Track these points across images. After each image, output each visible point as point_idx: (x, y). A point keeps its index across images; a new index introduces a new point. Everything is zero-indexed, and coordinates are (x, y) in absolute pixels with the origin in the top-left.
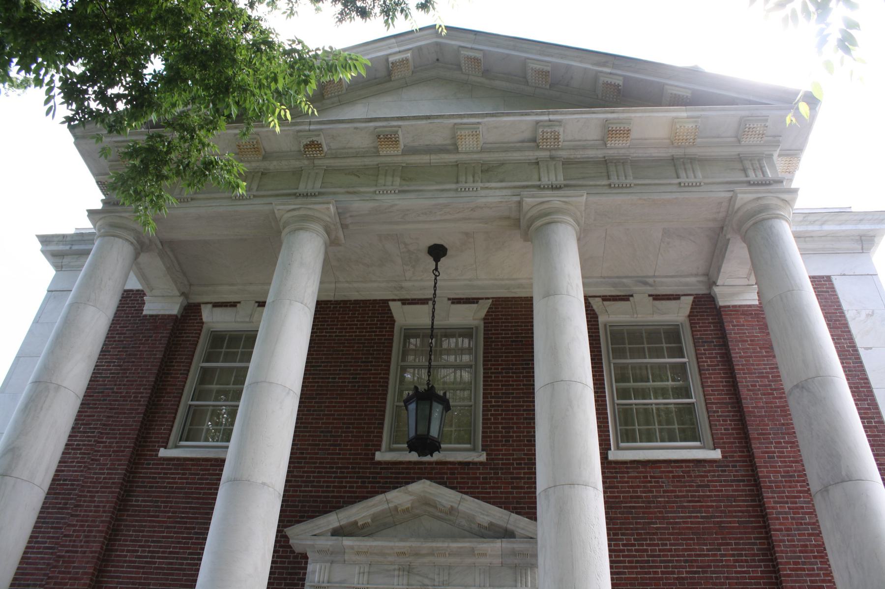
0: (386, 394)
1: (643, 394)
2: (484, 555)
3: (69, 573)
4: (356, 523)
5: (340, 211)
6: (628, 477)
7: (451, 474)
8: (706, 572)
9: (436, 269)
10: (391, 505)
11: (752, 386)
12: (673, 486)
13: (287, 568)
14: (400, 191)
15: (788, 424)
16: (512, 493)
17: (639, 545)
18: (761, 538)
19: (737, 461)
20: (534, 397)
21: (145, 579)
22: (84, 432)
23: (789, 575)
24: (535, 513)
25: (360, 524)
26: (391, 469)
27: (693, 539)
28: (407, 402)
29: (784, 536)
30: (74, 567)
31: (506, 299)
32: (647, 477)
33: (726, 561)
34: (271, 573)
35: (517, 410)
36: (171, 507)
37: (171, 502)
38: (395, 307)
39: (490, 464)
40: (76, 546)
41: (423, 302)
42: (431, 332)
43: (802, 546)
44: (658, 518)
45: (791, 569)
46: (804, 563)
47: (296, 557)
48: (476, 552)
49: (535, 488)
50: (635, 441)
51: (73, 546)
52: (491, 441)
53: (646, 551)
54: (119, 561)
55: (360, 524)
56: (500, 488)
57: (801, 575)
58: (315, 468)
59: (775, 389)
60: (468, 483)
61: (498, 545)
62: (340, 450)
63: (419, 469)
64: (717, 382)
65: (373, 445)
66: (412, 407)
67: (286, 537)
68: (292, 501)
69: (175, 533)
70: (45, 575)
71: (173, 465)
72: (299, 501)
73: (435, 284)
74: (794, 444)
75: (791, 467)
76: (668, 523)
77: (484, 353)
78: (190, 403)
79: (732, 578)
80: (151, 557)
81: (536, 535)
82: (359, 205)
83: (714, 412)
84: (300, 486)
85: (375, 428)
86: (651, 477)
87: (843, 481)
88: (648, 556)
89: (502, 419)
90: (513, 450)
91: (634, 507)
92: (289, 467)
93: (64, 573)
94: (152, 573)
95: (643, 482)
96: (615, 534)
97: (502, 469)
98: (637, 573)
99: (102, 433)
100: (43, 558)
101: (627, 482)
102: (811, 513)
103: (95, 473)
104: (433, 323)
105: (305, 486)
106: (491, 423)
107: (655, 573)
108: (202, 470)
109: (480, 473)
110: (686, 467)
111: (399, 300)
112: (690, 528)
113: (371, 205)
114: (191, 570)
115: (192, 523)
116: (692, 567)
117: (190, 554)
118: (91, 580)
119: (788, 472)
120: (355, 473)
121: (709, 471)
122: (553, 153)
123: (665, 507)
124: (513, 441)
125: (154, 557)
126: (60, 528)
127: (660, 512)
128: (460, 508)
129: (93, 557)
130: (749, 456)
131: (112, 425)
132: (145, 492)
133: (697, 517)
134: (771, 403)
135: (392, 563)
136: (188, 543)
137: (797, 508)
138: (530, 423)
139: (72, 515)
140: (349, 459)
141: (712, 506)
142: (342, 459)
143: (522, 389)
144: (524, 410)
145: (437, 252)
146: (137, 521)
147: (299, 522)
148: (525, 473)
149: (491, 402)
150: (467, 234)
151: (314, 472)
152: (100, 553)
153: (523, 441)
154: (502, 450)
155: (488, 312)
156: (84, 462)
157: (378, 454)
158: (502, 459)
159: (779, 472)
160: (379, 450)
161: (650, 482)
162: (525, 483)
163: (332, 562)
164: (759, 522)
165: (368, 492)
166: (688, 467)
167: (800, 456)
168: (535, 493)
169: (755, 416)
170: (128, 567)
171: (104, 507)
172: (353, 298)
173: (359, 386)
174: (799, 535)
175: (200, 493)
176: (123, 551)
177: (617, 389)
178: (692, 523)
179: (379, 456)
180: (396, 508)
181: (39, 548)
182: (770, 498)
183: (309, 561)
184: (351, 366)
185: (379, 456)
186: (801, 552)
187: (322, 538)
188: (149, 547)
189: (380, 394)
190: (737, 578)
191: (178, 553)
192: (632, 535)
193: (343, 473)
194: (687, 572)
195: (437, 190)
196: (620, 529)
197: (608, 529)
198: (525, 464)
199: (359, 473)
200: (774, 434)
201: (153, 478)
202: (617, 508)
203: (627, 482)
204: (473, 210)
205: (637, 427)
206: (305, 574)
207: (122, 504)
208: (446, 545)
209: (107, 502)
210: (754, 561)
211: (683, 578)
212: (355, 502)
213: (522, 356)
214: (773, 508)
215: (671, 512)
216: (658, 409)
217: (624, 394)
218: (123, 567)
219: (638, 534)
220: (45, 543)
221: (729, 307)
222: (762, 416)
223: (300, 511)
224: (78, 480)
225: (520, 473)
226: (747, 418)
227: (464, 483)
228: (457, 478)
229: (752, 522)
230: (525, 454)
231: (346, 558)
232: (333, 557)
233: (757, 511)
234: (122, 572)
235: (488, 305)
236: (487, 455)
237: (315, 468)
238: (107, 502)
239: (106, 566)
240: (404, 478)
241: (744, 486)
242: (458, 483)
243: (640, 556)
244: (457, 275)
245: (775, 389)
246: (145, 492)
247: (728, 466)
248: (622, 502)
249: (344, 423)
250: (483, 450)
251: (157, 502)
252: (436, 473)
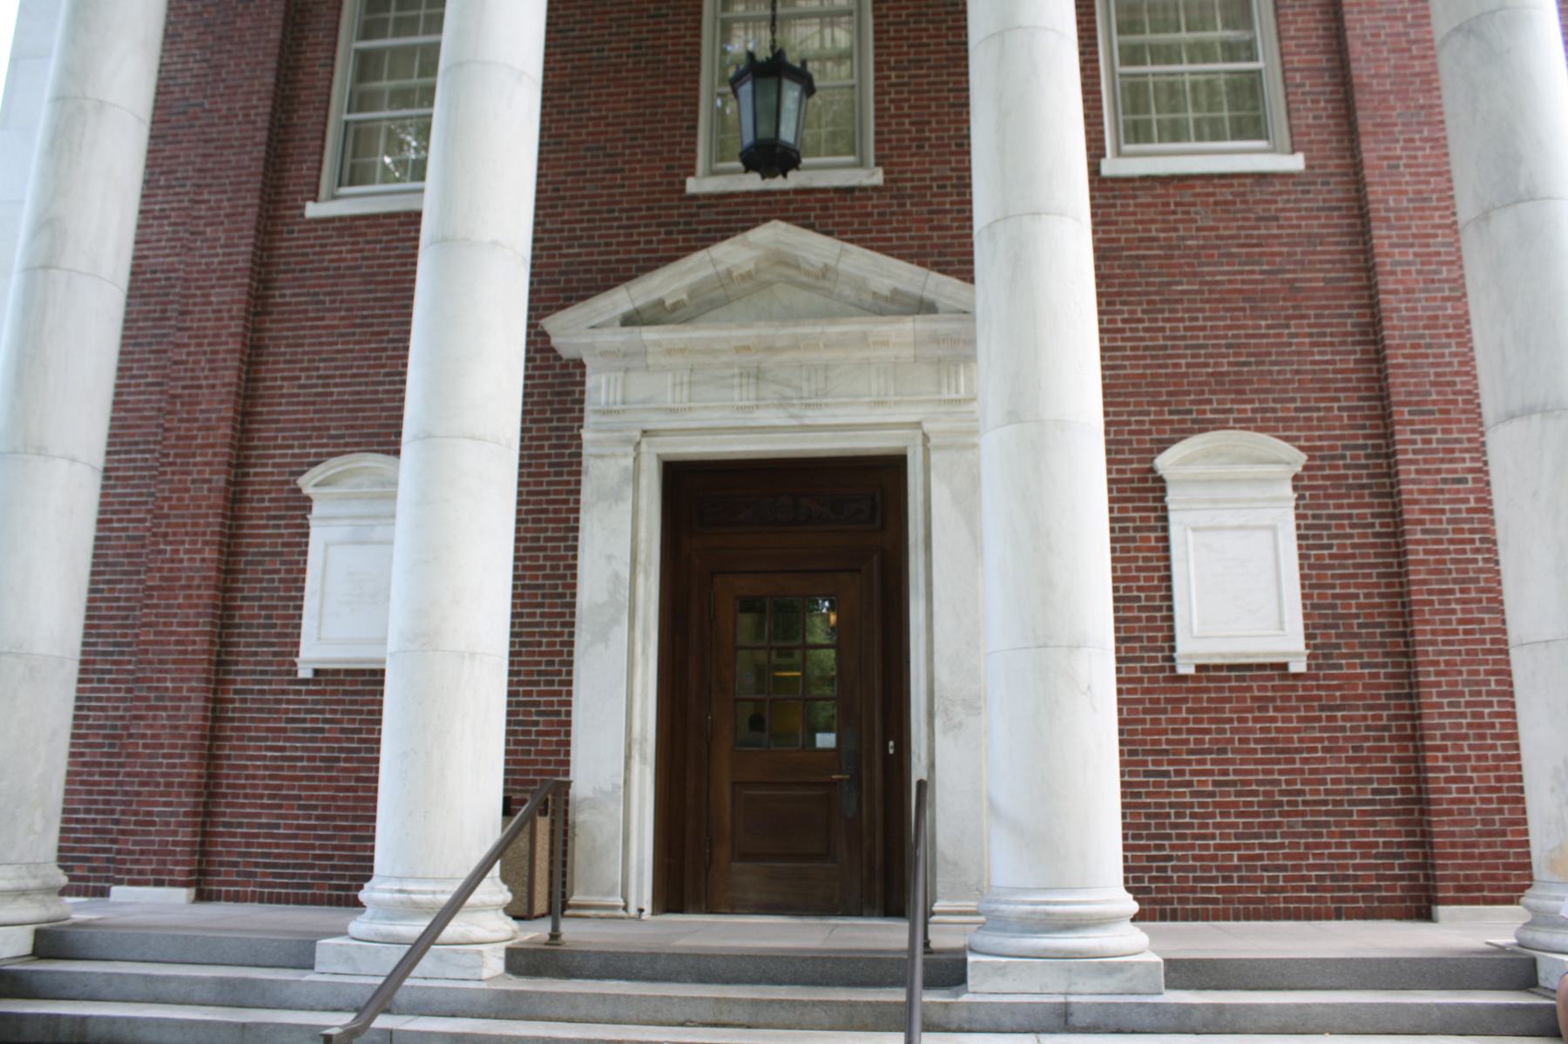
0: (697, 74)
1: (1168, 54)
2: (885, 344)
3: (196, 420)
4: (661, 302)
6: (1136, 205)
8: (1262, 363)
10: (721, 268)
11: (1373, 35)
12: (1215, 220)
13: (552, 385)
15: (1431, 106)
16: (930, 238)
17: (1151, 320)
18: (1360, 306)
19: (1332, 175)
20: (967, 66)
21: (320, 420)
22: (169, 187)
23: (1401, 366)
24: (971, 272)
25: (668, 303)
27: (1243, 309)
28: (735, 83)
29: (1401, 301)
30: (202, 411)
32: (1168, 204)
33: (1298, 344)
34: (526, 395)
36: (342, 301)
37: (340, 293)
39: (891, 189)
40: (198, 378)
43: (1430, 318)
45: (1406, 356)
46: (1429, 346)
47: (565, 366)
48: (871, 340)
49: (971, 228)
50: (1149, 140)
51: (192, 378)
52: (891, 149)
53: (1163, 329)
54: (272, 396)
55: (668, 303)
56: (908, 230)
57: (1421, 366)
58: (582, 213)
59: (1415, 42)
60: (851, 224)
61: (909, 327)
64: (1307, 30)
65: (682, 167)
66: (746, 89)
67: (545, 334)
68: (549, 274)
69: (356, 343)
70: (158, 426)
71: (334, 229)
72: (561, 273)
74: (1439, 143)
75: (1428, 183)
76: (1201, 283)
78: (346, 117)
79: (1306, 372)
80: (324, 386)
81: (973, 306)
83: (1298, 86)
84: (560, 248)
86: (1177, 204)
87: (1519, 201)
88: (1165, 338)
91: (1144, 257)
92: (536, 216)
93: (187, 420)
94: (330, 411)
95: (1162, 213)
96: (1108, 303)
97: (911, 196)
98: (1145, 367)
99: (199, 186)
100: (148, 401)
101: (1134, 214)
102: (1452, 263)
103: (202, 256)
105: (569, 247)
108: (385, 234)
109: (874, 206)
110: (1240, 185)
112: (1240, 291)
114: (393, 400)
115: (383, 324)
116: (1240, 355)
117: (387, 375)
118: (234, 428)
119: (1420, 192)
120: (652, 217)
121: (1280, 193)
123: (1197, 256)
125: (328, 385)
126: (165, 351)
127: (1191, 265)
128: (841, 266)
129: (229, 393)
130: (1355, 165)
131: (212, 170)
132: (294, 279)
133: (1252, 272)
134: (1405, 67)
135: (729, 365)
136: (380, 358)
137: (1429, 254)
138: (960, 114)
139: (179, 329)
141: (1280, 254)
142: (629, 194)
144: (950, 90)
146: (288, 329)
147: (562, 308)
151: (581, 221)
152: (238, 386)
153: (949, 145)
154: (910, 164)
156: (179, 239)
158: (912, 180)
159: (1405, 192)
160: (693, 174)
161: (1174, 213)
162: (953, 220)
163: (627, 370)
164: (1360, 279)
165: (678, 249)
166: (1244, 185)
167: (1448, 163)
168: (970, 236)
169: (1372, 93)
170: (288, 404)
171: (230, 310)
174: (1427, 299)
175: (387, 274)
176: (275, 379)
177: (1121, 48)
178: (1243, 282)
179: (693, 186)
180: (729, 272)
181: (138, 385)
182: (1382, 236)
183: (588, 370)
185: (693, 186)
186: (1426, 327)
187: (606, 330)
188: (317, 369)
189: (686, 74)
190: (1314, 372)
191: (366, 375)
192: (1140, 303)
194: (1230, 364)
196: (1119, 294)
197: (1099, 295)
200: (1404, 124)
201: (304, 255)
202: (1115, 258)
203: (1134, 214)
205: (1154, 116)
206: (582, 393)
207: (259, 304)
208: (818, 329)
209: (233, 302)
210: (1344, 343)
211: (1222, 374)
212: (657, 267)
214: (1387, 255)
215: (1208, 264)
216: (1194, 86)
217: (1132, 55)
218: (280, 404)
219: (1149, 302)
220: (146, 376)
222: (1384, 92)
223: (564, 290)
224: (175, 271)
226: (1358, 96)
227: (846, 224)
228: (833, 216)
229: (1348, 279)
230: (952, 170)
231: (650, 361)
232: (629, 360)
233: (1358, 261)
234: (281, 413)
236: (886, 173)
237: (582, 213)
238: (233, 302)
239: (253, 405)
241: (1340, 217)
242: (836, 224)
243: (1152, 339)
245: (1415, 42)
246: (294, 279)
247: (1314, 183)
248: (1123, 249)
249: (625, 132)
250: (877, 164)
251: (317, 294)
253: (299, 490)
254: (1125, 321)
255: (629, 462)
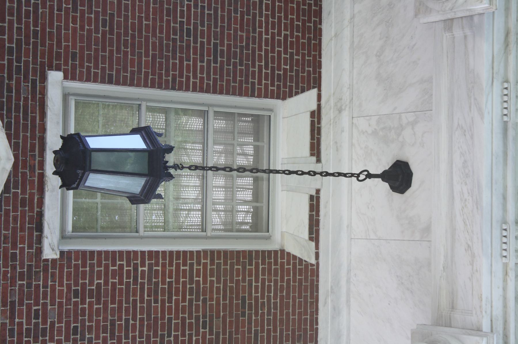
5: (476, 19)
7: (23, 200)
9: (370, 176)
14: (506, 123)
26: (34, 98)
31: (314, 288)
35: (127, 309)
38: (306, 100)
41: (315, 149)
42: (261, 172)
52: (76, 266)
62: (67, 9)
63: (33, 146)
65: (74, 67)
66: (137, 142)
73: (345, 175)
77: (225, 252)
85: (104, 69)
89: (114, 284)
90: (60, 304)
97: (29, 285)
104: (277, 172)
106: (107, 267)
109: (22, 250)
111: (319, 106)
113: (484, 73)
120: (27, 37)
124: (76, 304)
140: (51, 26)
143: (163, 318)
145: (399, 177)
148: (20, 324)
149: (143, 265)
150: (427, 230)
154: (61, 284)
155: (295, 257)
157: (60, 75)
158: (45, 286)
160: (66, 78)
172: (325, 27)
173: (174, 40)
184: (209, 27)
185: (55, 77)
193: (27, 16)
195: (505, 188)
198: (36, 325)
199: (27, 44)
204: (469, 248)
213: (218, 317)
225: (20, 317)
230: (53, 324)
235: (305, 258)
236: (54, 261)
240: (17, 122)
244: (359, 211)
249: (112, 16)
250: (62, 253)
252: (24, 174)
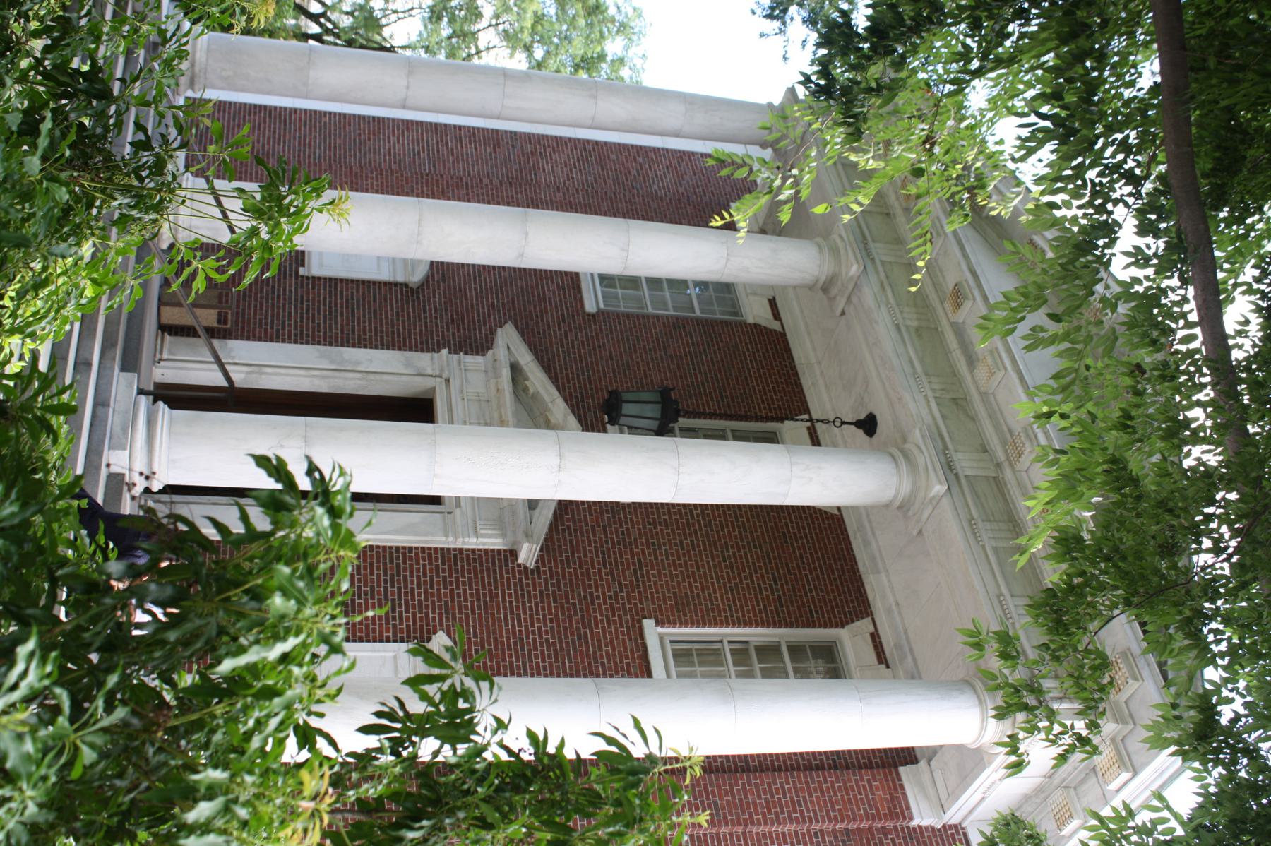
4: (527, 379)
9: (843, 423)
44: (577, 664)
82: (869, 294)
91: (587, 642)
107: (510, 656)
122: (1006, 464)
160: (657, 624)
172: (803, 381)
179: (648, 624)
185: (648, 624)
192: (553, 637)
196: (558, 625)
221: (900, 779)
253: (435, 633)
254: (539, 628)
255: (429, 371)
